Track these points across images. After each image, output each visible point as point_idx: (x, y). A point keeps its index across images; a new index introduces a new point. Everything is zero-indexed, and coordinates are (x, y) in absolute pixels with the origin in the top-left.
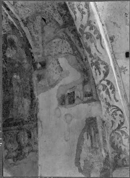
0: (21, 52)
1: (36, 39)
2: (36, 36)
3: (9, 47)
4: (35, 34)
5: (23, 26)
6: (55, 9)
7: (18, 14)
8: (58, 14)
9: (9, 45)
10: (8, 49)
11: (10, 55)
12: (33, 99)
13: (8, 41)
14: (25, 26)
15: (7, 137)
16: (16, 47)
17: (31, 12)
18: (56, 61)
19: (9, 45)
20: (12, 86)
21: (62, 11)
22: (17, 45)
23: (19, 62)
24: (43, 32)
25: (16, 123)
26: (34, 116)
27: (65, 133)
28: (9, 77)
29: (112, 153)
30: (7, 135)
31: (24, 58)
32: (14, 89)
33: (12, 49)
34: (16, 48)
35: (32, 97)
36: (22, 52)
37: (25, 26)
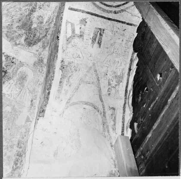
1: (63, 92)
3: (14, 81)
5: (59, 68)
6: (107, 75)
7: (64, 51)
8: (106, 82)
13: (18, 72)
16: (23, 86)
17: (81, 59)
21: (113, 81)
22: (26, 85)
24: (77, 89)
29: (66, 77)
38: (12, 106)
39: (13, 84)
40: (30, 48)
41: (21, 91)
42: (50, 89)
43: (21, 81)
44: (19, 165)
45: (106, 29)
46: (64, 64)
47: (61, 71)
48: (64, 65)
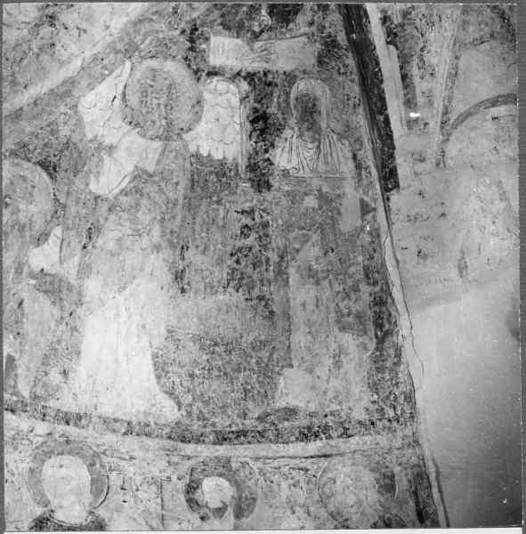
0: (334, 155)
2: (425, 90)
3: (293, 129)
4: (422, 78)
9: (292, 121)
10: (287, 133)
11: (289, 161)
12: (387, 334)
13: (292, 103)
14: (388, 43)
15: (275, 486)
16: (318, 131)
18: (494, 188)
19: (292, 121)
20: (287, 281)
22: (323, 125)
23: (320, 190)
25: (309, 428)
26: (396, 398)
27: (130, 518)
28: (274, 245)
30: (276, 478)
31: (344, 179)
32: (291, 295)
33: (300, 136)
34: (317, 136)
35: (379, 326)
36: (340, 154)
37: (388, 43)
38: (316, 193)
39: (295, 137)
40: (291, 25)
41: (320, 143)
42: (386, 109)
43: (308, 120)
44: (387, 326)
45: (166, 145)
46: (391, 24)
47: (391, 47)
48: (393, 26)
